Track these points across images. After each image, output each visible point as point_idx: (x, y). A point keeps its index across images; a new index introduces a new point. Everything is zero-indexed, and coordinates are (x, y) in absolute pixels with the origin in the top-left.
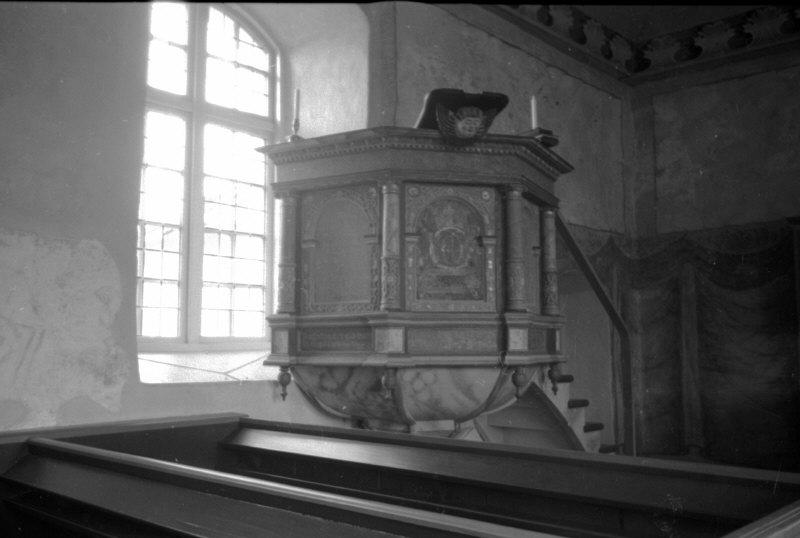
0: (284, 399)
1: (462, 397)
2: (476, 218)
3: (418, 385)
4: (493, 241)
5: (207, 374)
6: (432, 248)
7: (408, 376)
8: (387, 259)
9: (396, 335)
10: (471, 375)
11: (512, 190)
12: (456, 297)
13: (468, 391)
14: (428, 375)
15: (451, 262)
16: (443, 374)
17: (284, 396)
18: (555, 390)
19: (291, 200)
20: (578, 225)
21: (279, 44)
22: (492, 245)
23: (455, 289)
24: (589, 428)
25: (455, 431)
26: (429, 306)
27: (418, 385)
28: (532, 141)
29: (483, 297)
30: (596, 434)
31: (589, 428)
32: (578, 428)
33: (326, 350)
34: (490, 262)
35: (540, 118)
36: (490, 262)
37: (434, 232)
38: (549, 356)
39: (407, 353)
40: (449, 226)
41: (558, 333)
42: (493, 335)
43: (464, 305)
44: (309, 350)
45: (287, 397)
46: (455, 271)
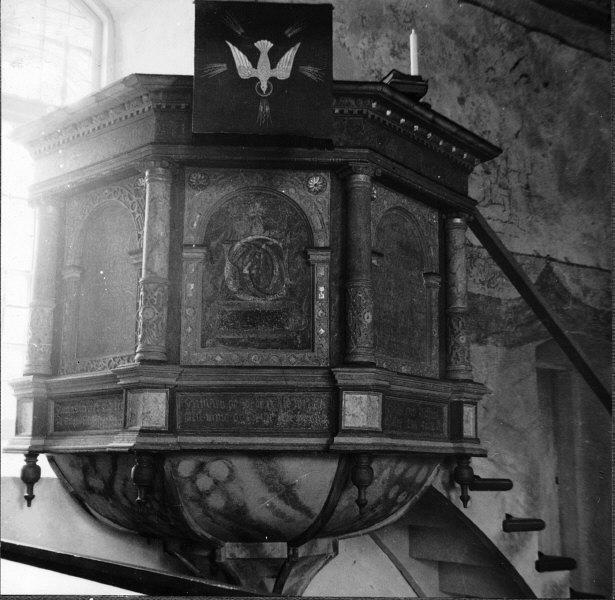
0: (29, 505)
1: (280, 505)
2: (299, 221)
3: (204, 482)
4: (325, 256)
5: (412, 572)
6: (228, 266)
7: (186, 467)
8: (144, 282)
9: (156, 401)
10: (293, 469)
11: (356, 173)
12: (266, 345)
13: (288, 493)
14: (218, 468)
15: (261, 292)
16: (242, 465)
17: (29, 499)
18: (465, 499)
19: (51, 209)
20: (585, 267)
21: (108, 11)
22: (323, 262)
23: (264, 332)
24: (544, 564)
25: (288, 560)
26: (219, 359)
27: (204, 482)
28: (379, 88)
29: (309, 344)
30: (560, 576)
31: (544, 564)
32: (525, 565)
33: (80, 429)
34: (322, 289)
35: (421, 63)
36: (322, 289)
37: (232, 242)
38: (451, 445)
39: (172, 429)
40: (258, 233)
41: (468, 411)
42: (321, 403)
43: (274, 357)
44: (63, 429)
45: (33, 502)
46: (263, 303)
